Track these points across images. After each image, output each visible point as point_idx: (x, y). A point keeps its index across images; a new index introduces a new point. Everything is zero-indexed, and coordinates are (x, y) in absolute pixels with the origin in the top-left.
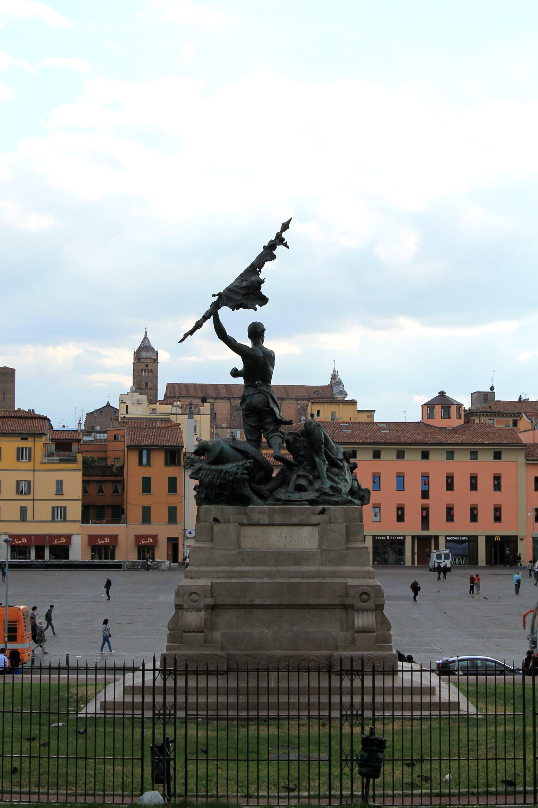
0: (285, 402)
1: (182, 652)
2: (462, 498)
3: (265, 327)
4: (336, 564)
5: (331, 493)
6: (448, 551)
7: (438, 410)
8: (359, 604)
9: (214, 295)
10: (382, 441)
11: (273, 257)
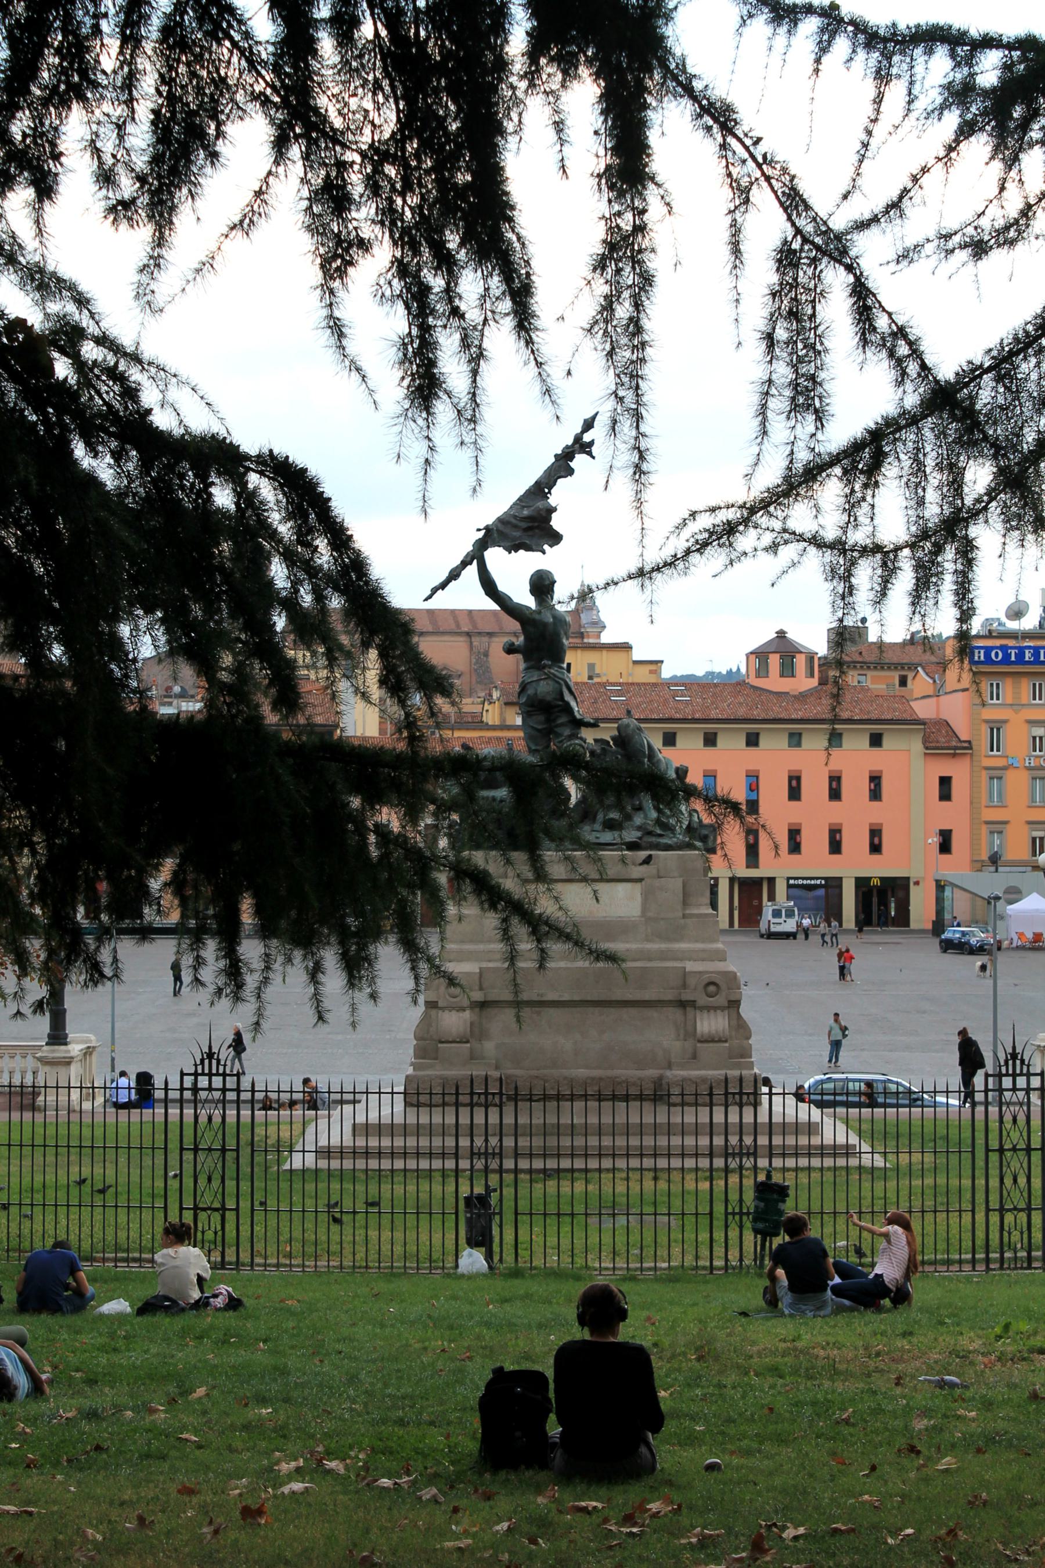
1: (436, 1071)
2: (815, 814)
4: (669, 940)
5: (659, 832)
7: (774, 661)
8: (703, 1000)
10: (678, 716)
11: (570, 472)
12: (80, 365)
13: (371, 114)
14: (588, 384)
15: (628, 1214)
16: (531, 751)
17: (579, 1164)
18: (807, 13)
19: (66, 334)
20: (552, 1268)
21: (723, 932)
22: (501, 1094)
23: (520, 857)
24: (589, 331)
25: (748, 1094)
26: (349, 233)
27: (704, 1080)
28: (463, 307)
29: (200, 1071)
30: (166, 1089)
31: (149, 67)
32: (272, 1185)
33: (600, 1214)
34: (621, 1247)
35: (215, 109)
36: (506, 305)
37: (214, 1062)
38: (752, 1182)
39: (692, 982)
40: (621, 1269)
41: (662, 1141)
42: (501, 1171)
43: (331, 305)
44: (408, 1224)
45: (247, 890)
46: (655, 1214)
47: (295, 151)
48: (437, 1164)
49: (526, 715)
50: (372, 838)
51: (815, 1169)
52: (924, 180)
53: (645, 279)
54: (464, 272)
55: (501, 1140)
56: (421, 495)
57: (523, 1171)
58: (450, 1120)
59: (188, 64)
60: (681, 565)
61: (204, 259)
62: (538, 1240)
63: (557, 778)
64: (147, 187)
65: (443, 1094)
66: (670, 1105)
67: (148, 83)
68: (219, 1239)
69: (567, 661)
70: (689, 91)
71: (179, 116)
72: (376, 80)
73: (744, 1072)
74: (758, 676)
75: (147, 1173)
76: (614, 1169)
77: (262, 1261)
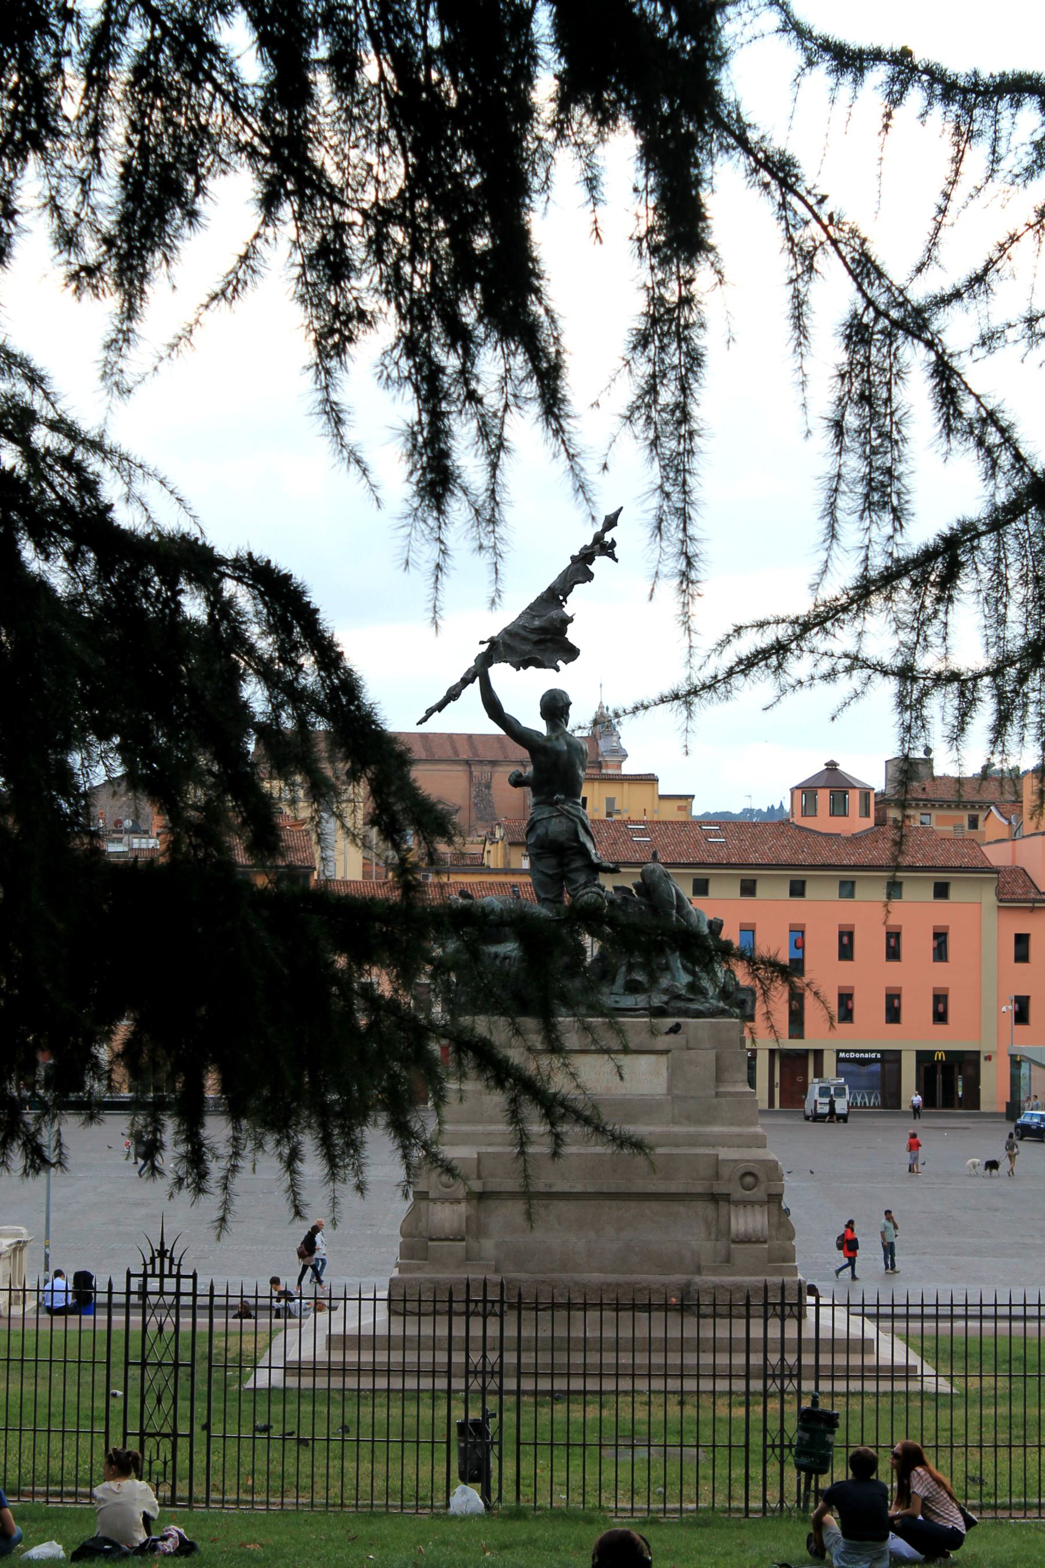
0: (500, 769)
1: (427, 1274)
2: (869, 976)
3: (571, 699)
4: (699, 1122)
6: (842, 1080)
7: (823, 797)
8: (738, 1193)
9: (482, 643)
10: (710, 860)
11: (589, 576)
12: (30, 454)
13: (375, 169)
14: (629, 478)
15: (649, 1446)
16: (541, 901)
17: (592, 1385)
18: (874, 60)
19: (14, 417)
20: (559, 1508)
21: (762, 1112)
22: (502, 1302)
23: (529, 1023)
24: (628, 418)
25: (791, 1305)
26: (348, 305)
27: (739, 1287)
28: (481, 390)
29: (150, 1271)
30: (110, 1293)
31: (117, 113)
32: (232, 1408)
33: (617, 1446)
34: (640, 1484)
35: (194, 161)
36: (531, 388)
37: (167, 1262)
38: (794, 1408)
39: (725, 1171)
40: (641, 1510)
41: (690, 1359)
42: (500, 1392)
43: (327, 387)
44: (391, 1455)
45: (212, 1063)
46: (682, 1446)
47: (287, 210)
48: (426, 1383)
49: (535, 858)
50: (358, 1003)
51: (868, 1394)
52: (1013, 250)
53: (693, 359)
54: (482, 350)
55: (501, 1356)
56: (431, 605)
57: (526, 1392)
58: (442, 1331)
59: (164, 110)
60: (721, 688)
61: (181, 333)
62: (544, 1474)
63: (574, 934)
64: (114, 251)
65: (435, 1301)
66: (699, 1316)
67: (117, 132)
68: (169, 1470)
69: (583, 795)
70: (743, 142)
71: (151, 169)
72: (381, 131)
73: (787, 1279)
74: (804, 814)
75: (86, 1390)
76: (633, 1391)
77: (219, 1497)
